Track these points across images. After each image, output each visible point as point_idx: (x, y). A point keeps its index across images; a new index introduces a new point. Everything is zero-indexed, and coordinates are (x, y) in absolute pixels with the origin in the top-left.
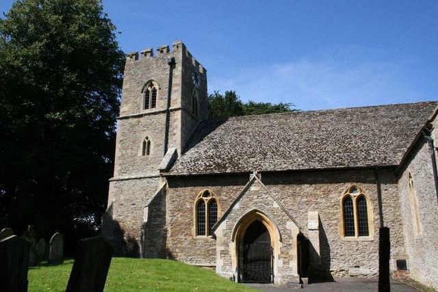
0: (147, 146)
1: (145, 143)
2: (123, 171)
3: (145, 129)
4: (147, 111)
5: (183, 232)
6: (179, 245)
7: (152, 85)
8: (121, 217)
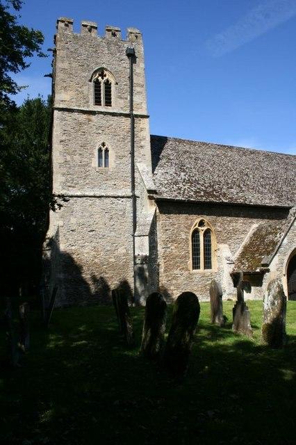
0: (103, 154)
1: (100, 150)
2: (68, 184)
3: (100, 132)
4: (102, 108)
5: (179, 266)
6: (174, 282)
7: (103, 75)
8: (73, 248)
